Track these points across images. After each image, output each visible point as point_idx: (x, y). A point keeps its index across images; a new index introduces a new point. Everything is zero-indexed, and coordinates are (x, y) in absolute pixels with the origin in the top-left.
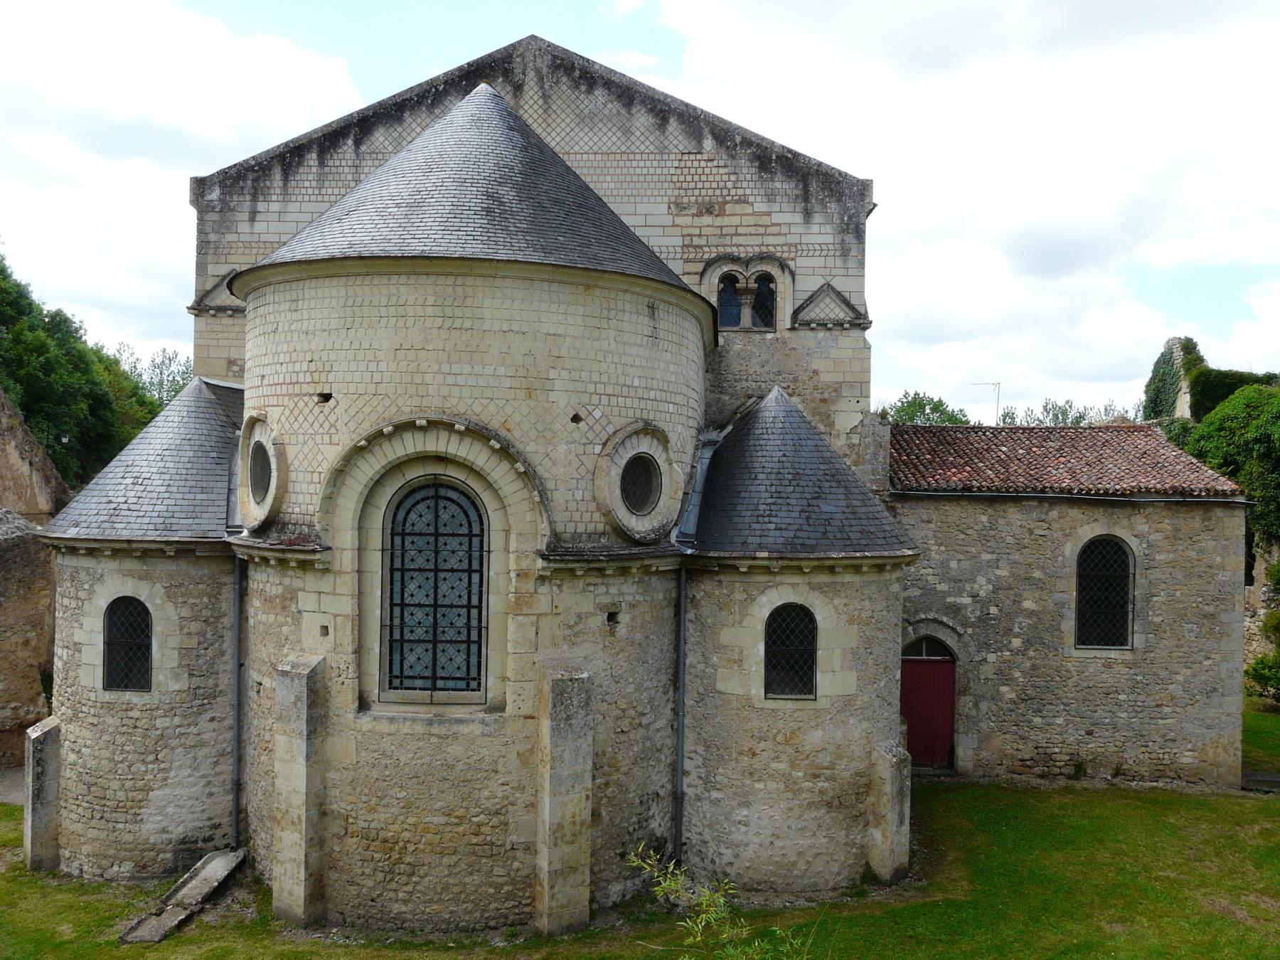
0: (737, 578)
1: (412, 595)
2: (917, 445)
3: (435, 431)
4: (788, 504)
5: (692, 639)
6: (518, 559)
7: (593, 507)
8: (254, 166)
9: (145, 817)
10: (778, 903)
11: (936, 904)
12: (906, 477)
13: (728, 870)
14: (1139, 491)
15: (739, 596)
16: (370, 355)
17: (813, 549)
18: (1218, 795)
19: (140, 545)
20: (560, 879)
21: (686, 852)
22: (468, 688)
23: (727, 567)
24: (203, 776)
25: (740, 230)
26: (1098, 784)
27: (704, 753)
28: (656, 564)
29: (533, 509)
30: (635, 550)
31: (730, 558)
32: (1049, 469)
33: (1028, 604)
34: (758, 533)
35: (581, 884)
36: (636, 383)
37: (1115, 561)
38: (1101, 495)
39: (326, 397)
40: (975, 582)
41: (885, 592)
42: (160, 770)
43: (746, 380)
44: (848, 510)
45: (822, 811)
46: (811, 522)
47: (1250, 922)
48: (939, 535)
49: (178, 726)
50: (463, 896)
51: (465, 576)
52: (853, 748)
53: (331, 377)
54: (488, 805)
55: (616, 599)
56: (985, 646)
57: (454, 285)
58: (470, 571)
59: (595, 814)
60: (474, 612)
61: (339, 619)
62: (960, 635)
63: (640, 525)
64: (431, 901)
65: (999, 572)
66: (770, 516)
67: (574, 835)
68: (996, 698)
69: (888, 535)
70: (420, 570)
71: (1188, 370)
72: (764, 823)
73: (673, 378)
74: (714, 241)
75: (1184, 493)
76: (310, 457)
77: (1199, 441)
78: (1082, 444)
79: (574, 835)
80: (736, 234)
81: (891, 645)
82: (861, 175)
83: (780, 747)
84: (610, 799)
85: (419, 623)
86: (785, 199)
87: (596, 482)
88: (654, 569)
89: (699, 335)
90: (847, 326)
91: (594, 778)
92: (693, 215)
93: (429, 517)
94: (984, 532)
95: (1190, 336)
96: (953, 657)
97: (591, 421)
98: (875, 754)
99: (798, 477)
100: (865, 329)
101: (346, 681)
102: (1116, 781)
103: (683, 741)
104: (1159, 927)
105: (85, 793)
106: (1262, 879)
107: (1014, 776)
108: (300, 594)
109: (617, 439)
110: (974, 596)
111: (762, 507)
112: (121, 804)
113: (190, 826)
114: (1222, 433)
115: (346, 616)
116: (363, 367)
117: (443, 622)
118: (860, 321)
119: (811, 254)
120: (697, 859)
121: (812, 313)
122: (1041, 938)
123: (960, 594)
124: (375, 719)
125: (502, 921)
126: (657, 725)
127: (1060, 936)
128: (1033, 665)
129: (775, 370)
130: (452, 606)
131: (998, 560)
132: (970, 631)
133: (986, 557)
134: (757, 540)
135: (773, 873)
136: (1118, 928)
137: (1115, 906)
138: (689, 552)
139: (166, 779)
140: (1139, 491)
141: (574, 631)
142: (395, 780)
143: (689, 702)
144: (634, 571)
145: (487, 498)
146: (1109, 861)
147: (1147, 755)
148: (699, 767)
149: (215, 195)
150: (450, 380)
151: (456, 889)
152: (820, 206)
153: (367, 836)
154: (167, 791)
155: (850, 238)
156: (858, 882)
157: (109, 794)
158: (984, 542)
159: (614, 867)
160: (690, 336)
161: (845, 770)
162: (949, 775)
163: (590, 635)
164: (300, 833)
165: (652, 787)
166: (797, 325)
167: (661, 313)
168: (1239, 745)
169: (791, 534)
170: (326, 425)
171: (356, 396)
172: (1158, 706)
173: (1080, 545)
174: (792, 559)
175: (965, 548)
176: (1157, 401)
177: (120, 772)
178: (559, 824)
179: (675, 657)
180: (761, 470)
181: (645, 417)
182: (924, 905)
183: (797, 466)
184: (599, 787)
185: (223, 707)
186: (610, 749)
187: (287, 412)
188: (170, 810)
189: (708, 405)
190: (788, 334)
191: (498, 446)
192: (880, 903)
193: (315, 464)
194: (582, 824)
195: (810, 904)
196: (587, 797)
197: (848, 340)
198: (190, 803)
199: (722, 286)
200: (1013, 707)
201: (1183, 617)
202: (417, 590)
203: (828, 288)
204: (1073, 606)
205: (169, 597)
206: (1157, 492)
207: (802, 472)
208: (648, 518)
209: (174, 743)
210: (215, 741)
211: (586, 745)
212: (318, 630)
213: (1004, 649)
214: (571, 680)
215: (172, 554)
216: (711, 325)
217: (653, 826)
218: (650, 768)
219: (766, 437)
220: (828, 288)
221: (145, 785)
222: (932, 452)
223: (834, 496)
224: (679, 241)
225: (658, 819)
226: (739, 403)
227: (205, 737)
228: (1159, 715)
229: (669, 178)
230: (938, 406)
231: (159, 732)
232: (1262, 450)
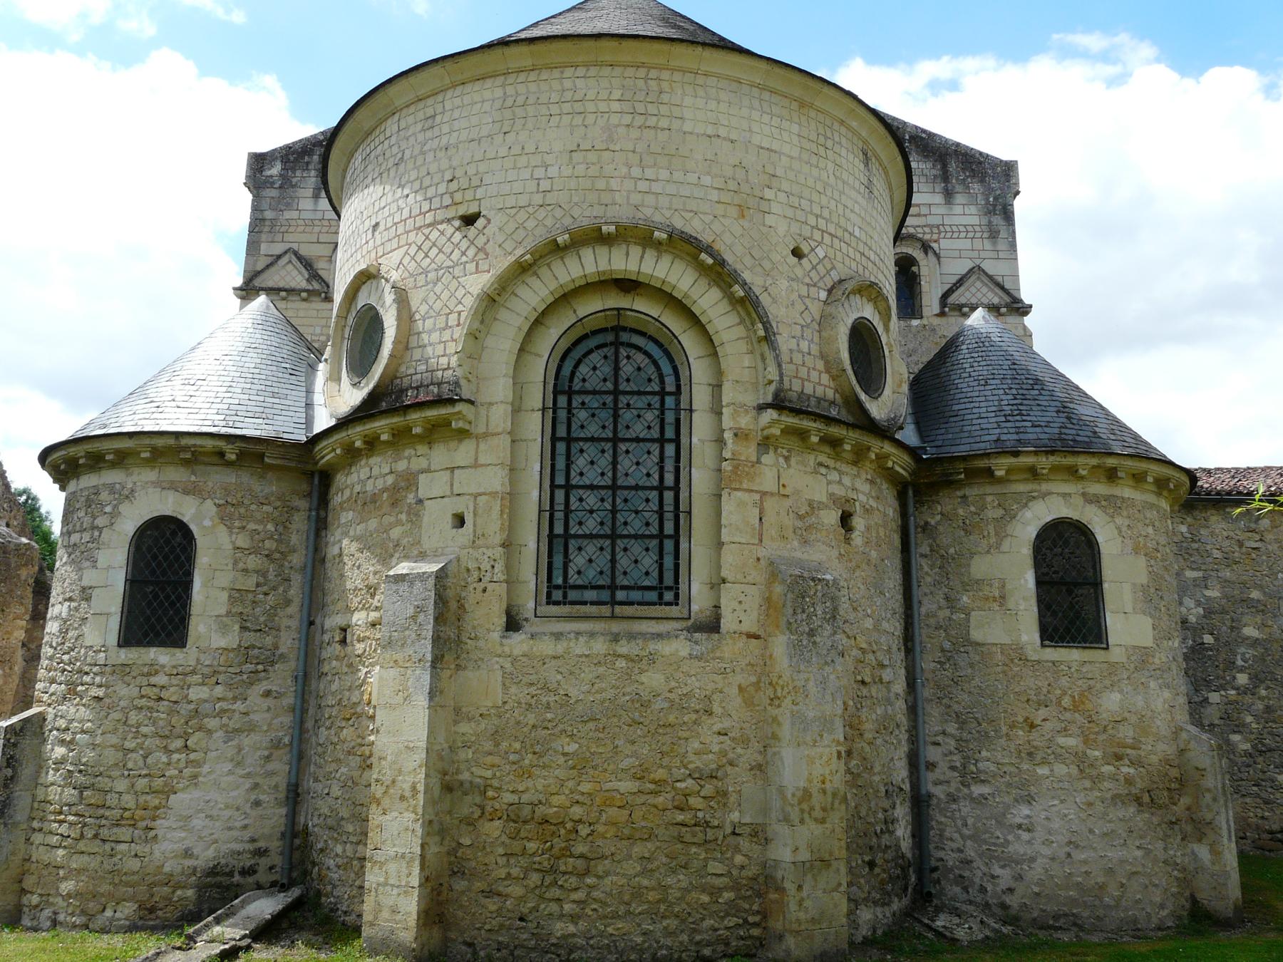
1: (581, 474)
3: (624, 246)
4: (1039, 405)
5: (929, 579)
7: (820, 365)
8: (323, 141)
9: (160, 833)
13: (1008, 899)
15: (993, 513)
16: (536, 160)
20: (809, 876)
21: (938, 881)
22: (661, 602)
24: (248, 775)
27: (957, 733)
29: (752, 353)
33: (1250, 631)
35: (835, 890)
39: (469, 220)
42: (189, 763)
45: (1132, 810)
50: (663, 907)
51: (655, 448)
54: (698, 764)
57: (646, 79)
58: (662, 441)
60: (668, 496)
61: (482, 500)
64: (615, 916)
65: (1208, 593)
70: (592, 439)
82: (1005, 157)
83: (1068, 715)
90: (1003, 310)
93: (607, 369)
94: (1185, 545)
101: (490, 587)
105: (74, 800)
112: (127, 814)
113: (225, 848)
115: (493, 494)
116: (526, 174)
120: (957, 890)
124: (533, 636)
125: (720, 948)
128: (1267, 707)
130: (637, 488)
135: (1074, 901)
139: (195, 776)
141: (807, 515)
142: (561, 727)
145: (690, 342)
148: (951, 753)
149: (275, 170)
150: (643, 186)
151: (652, 896)
152: (961, 187)
153: (513, 817)
154: (196, 794)
155: (998, 220)
157: (112, 800)
159: (862, 881)
163: (824, 533)
169: (1057, 431)
170: (471, 253)
171: (514, 211)
177: (130, 765)
178: (805, 790)
185: (281, 678)
188: (197, 823)
190: (936, 321)
198: (228, 813)
203: (976, 270)
209: (212, 723)
210: (270, 725)
212: (448, 520)
214: (813, 579)
215: (233, 457)
220: (976, 270)
221: (166, 785)
227: (255, 717)
231: (192, 706)
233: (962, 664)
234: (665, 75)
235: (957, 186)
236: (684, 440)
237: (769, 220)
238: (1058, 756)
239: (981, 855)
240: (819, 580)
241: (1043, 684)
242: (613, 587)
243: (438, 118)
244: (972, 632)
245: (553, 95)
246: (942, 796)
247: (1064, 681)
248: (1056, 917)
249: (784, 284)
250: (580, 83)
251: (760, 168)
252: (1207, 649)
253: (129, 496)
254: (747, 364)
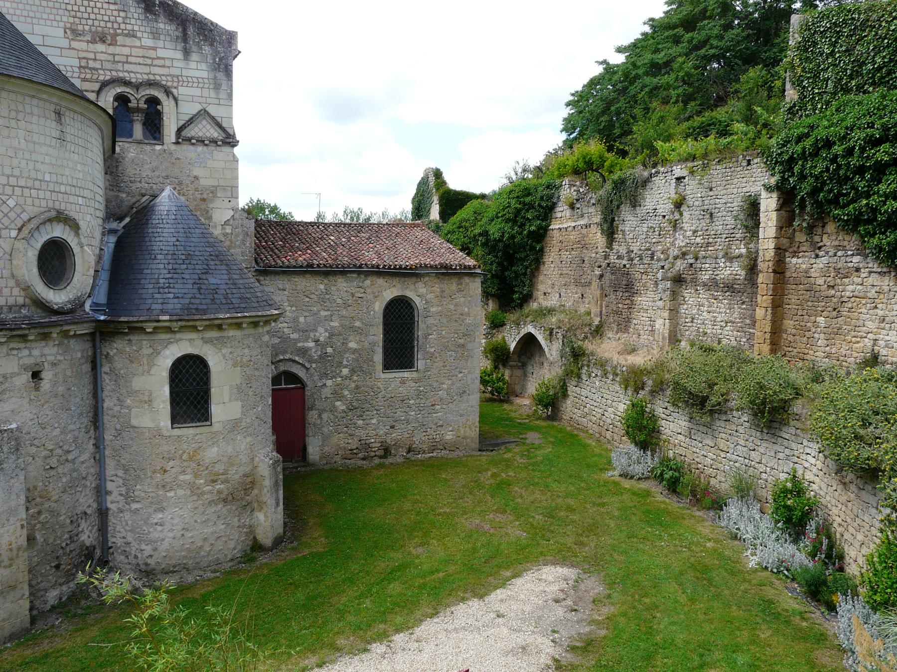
0: (144, 337)
2: (272, 235)
4: (183, 278)
5: (108, 388)
7: (12, 283)
10: (190, 579)
11: (305, 557)
12: (266, 257)
13: (149, 561)
14: (421, 266)
15: (146, 351)
17: (205, 312)
18: (467, 456)
21: (113, 553)
23: (135, 329)
25: (130, 59)
26: (399, 460)
28: (73, 329)
30: (54, 319)
31: (138, 322)
32: (363, 252)
33: (352, 345)
34: (160, 301)
35: (21, 598)
36: (47, 178)
37: (406, 313)
38: (396, 269)
40: (316, 331)
41: (259, 342)
43: (140, 182)
44: (228, 282)
45: (220, 506)
46: (202, 291)
47: (492, 531)
48: (292, 299)
52: (241, 457)
55: (39, 360)
56: (324, 375)
59: (31, 539)
62: (307, 369)
63: (57, 298)
65: (332, 324)
66: (169, 287)
68: (333, 410)
69: (260, 300)
71: (437, 189)
72: (175, 522)
73: (81, 175)
74: (108, 66)
75: (446, 267)
77: (447, 235)
78: (383, 235)
79: (11, 559)
80: (127, 62)
81: (264, 380)
83: (185, 464)
84: (43, 524)
86: (168, 38)
87: (14, 262)
88: (72, 333)
89: (101, 142)
91: (27, 509)
92: (88, 42)
94: (322, 296)
95: (439, 167)
96: (303, 384)
98: (257, 459)
99: (190, 257)
100: (234, 146)
102: (408, 456)
103: (105, 469)
104: (444, 544)
106: (495, 503)
107: (346, 461)
109: (32, 225)
110: (317, 341)
111: (161, 281)
114: (461, 230)
118: (229, 140)
120: (122, 557)
121: (193, 132)
122: (375, 567)
123: (307, 341)
126: (82, 459)
127: (387, 563)
128: (357, 386)
129: (164, 174)
131: (331, 315)
132: (314, 365)
133: (323, 313)
134: (160, 307)
135: (185, 557)
136: (420, 550)
137: (417, 536)
138: (102, 318)
140: (421, 266)
143: (108, 437)
144: (55, 335)
146: (410, 508)
147: (427, 437)
155: (221, 76)
156: (249, 552)
158: (322, 303)
159: (51, 577)
160: (94, 141)
161: (235, 474)
162: (303, 466)
165: (80, 508)
166: (180, 140)
167: (67, 120)
168: (477, 424)
169: (187, 301)
172: (433, 405)
173: (385, 303)
174: (188, 321)
175: (309, 308)
176: (420, 208)
179: (94, 403)
180: (159, 252)
181: (57, 206)
182: (298, 559)
183: (188, 248)
184: (32, 516)
186: (41, 484)
189: (108, 201)
190: (173, 147)
192: (266, 564)
194: (19, 549)
195: (214, 575)
196: (22, 526)
197: (221, 153)
199: (116, 104)
200: (344, 415)
201: (446, 347)
203: (204, 113)
204: (381, 344)
206: (431, 267)
207: (192, 253)
208: (64, 291)
211: (18, 484)
213: (337, 376)
216: (110, 134)
217: (82, 539)
218: (78, 494)
219: (162, 226)
220: (204, 113)
222: (283, 239)
223: (219, 272)
224: (76, 63)
225: (87, 533)
226: (134, 200)
228: (433, 411)
229: (63, 6)
230: (274, 209)
232: (483, 241)
233: (126, 438)
235: (193, 46)
238: (179, 486)
239: (135, 540)
240: (6, 430)
241: (172, 448)
244: (132, 421)
246: (115, 509)
248: (174, 567)
252: (328, 356)
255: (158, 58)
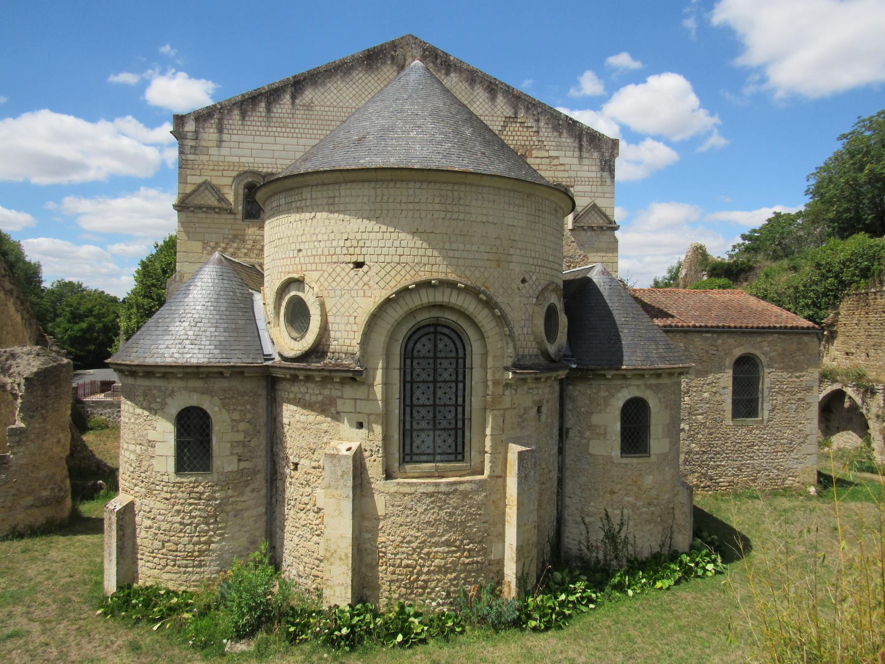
0: (603, 382)
6: (494, 373)
7: (532, 338)
15: (603, 394)
19: (207, 369)
22: (456, 460)
39: (359, 265)
49: (231, 497)
51: (453, 385)
53: (364, 251)
57: (453, 190)
60: (460, 409)
61: (372, 417)
67: (528, 552)
76: (347, 305)
85: (423, 417)
87: (535, 322)
93: (429, 346)
97: (531, 282)
108: (338, 401)
115: (378, 415)
117: (439, 416)
119: (579, 183)
121: (198, 200)
142: (413, 525)
145: (471, 333)
155: (606, 174)
164: (347, 565)
170: (361, 284)
171: (383, 265)
173: (734, 359)
187: (326, 275)
191: (481, 296)
193: (351, 311)
202: (422, 396)
203: (594, 207)
205: (223, 406)
234: (462, 188)
236: (468, 382)
237: (512, 266)
242: (434, 454)
243: (337, 200)
245: (403, 198)
247: (629, 473)
249: (517, 299)
250: (417, 191)
251: (508, 238)
253: (172, 394)
254: (499, 346)
255: (561, 164)
